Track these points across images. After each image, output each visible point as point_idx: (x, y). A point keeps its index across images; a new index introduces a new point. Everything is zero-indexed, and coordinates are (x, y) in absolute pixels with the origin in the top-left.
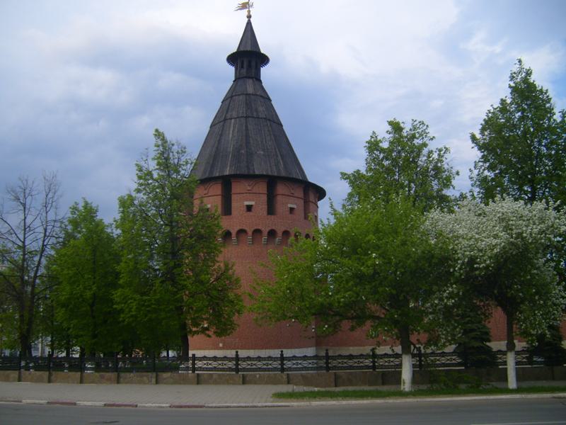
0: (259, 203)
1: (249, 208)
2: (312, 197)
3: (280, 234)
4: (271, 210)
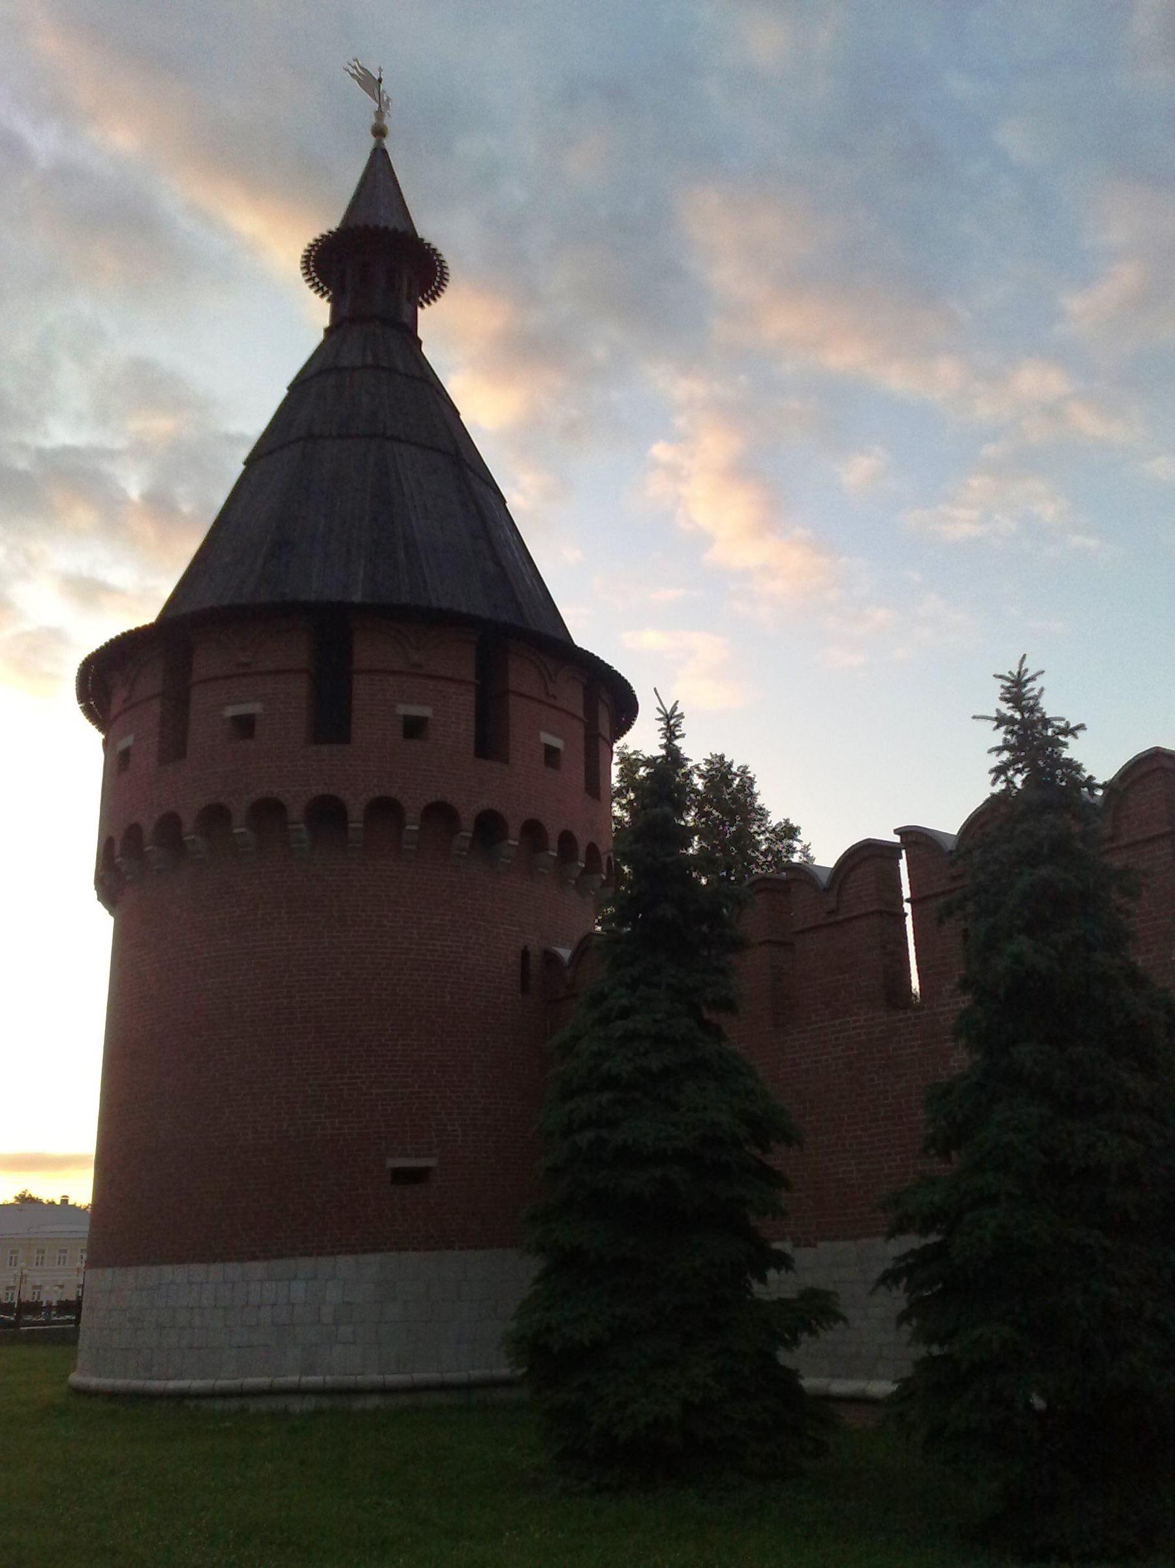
0: (453, 714)
1: (414, 728)
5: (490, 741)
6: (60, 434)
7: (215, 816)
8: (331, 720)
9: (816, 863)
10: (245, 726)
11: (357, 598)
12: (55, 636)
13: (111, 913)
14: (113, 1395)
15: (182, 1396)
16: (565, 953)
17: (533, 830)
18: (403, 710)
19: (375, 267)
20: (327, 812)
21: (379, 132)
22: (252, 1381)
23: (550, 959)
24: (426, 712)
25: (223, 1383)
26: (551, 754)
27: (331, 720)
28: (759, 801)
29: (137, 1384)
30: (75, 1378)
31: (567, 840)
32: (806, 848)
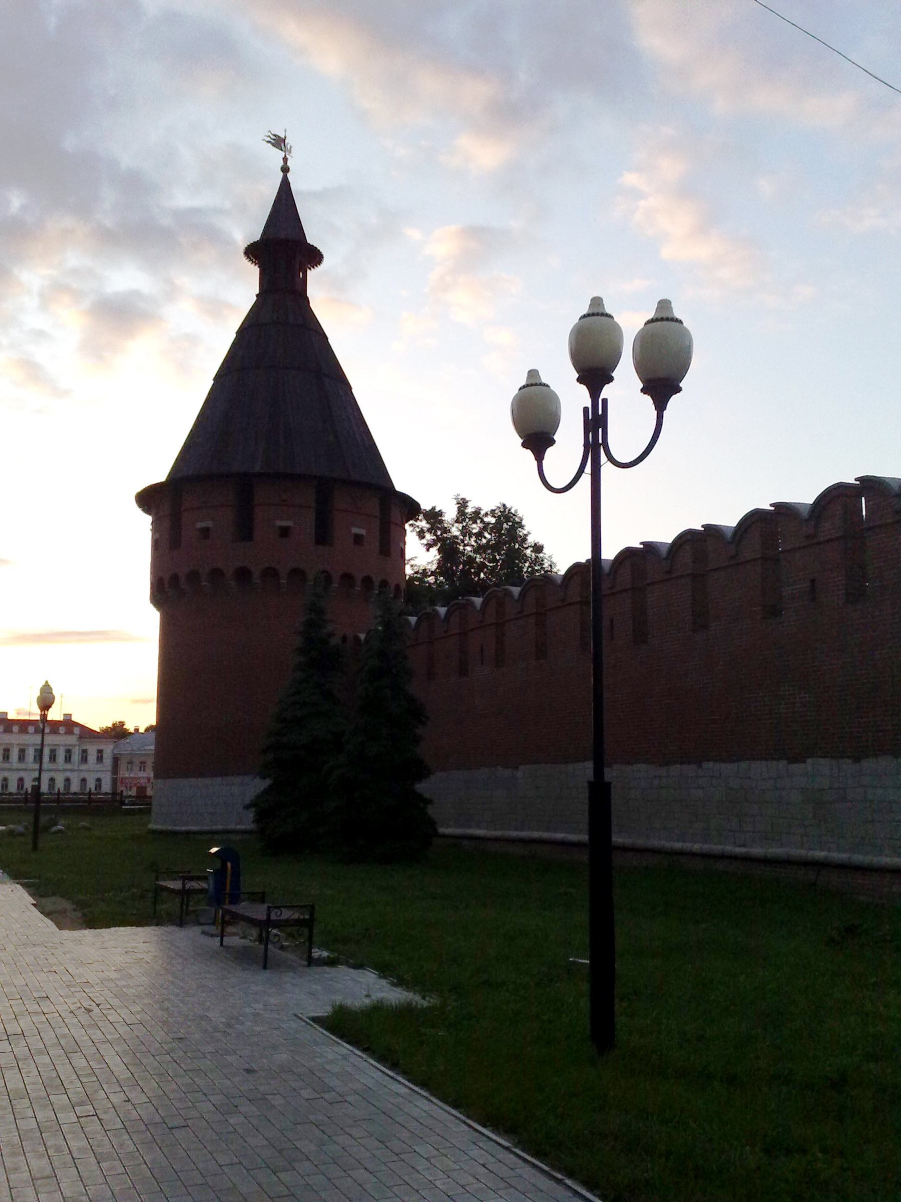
0: (304, 524)
1: (285, 532)
2: (396, 513)
3: (377, 583)
4: (323, 536)
5: (323, 534)
6: (182, 200)
7: (193, 576)
8: (245, 530)
9: (154, 723)
10: (206, 532)
11: (257, 468)
12: (192, 339)
13: (158, 610)
14: (161, 832)
15: (188, 833)
16: (362, 636)
17: (347, 578)
18: (279, 523)
19: (284, 251)
20: (243, 574)
21: (285, 170)
22: (214, 828)
23: (357, 639)
24: (289, 523)
25: (206, 828)
26: (358, 539)
27: (245, 530)
28: (110, 725)
29: (170, 828)
30: (152, 826)
31: (367, 581)
32: (550, 557)
